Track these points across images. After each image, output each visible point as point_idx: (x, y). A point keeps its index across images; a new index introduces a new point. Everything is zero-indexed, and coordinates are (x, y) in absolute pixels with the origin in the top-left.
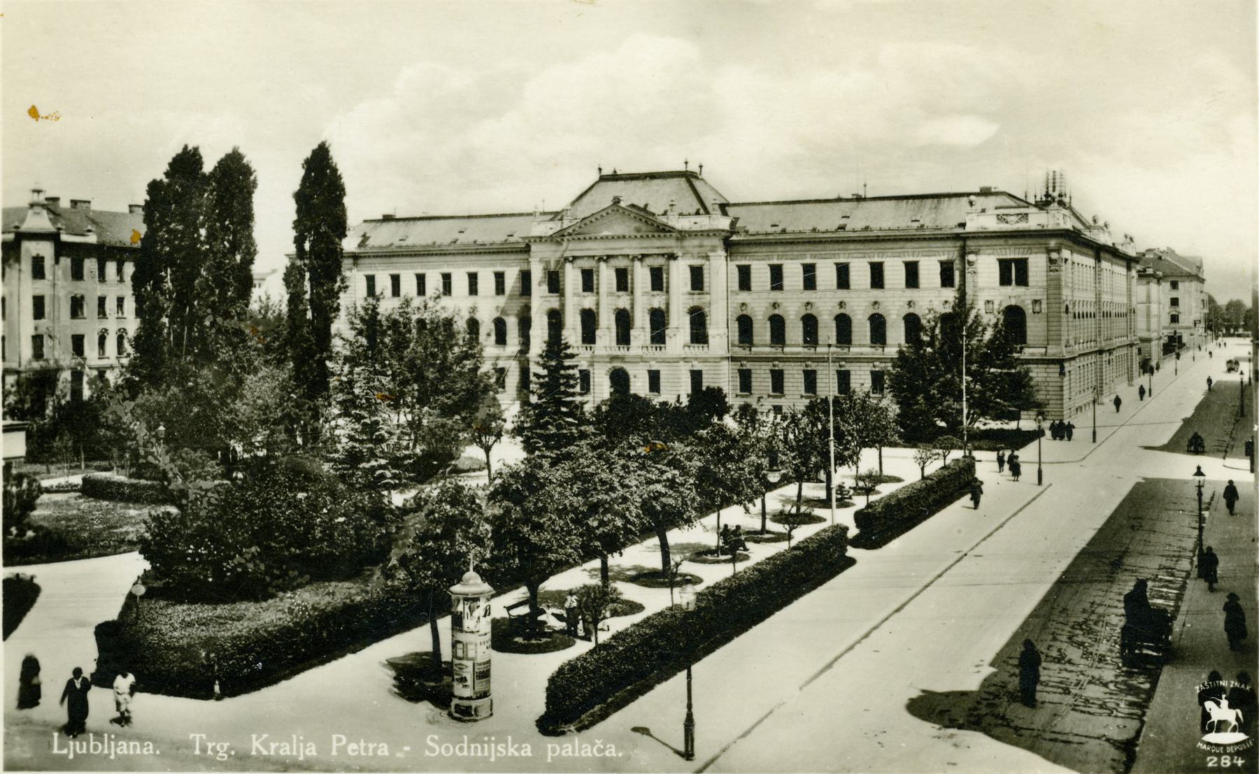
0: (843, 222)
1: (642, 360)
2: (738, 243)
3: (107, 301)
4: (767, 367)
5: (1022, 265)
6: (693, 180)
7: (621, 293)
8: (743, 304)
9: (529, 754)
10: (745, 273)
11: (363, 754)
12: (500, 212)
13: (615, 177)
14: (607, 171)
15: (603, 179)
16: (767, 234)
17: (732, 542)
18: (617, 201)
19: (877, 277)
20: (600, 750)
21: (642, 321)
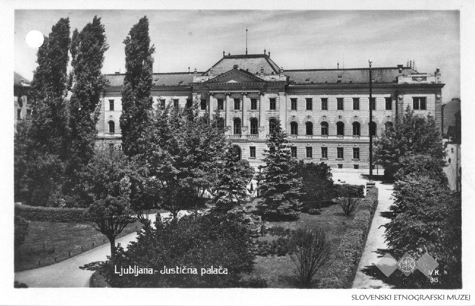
1: (247, 141)
2: (291, 88)
4: (304, 146)
5: (424, 100)
7: (236, 110)
8: (294, 116)
9: (196, 273)
10: (294, 101)
11: (177, 273)
12: (299, 69)
13: (230, 57)
14: (226, 54)
15: (225, 57)
16: (304, 84)
18: (236, 67)
20: (185, 271)
21: (247, 123)
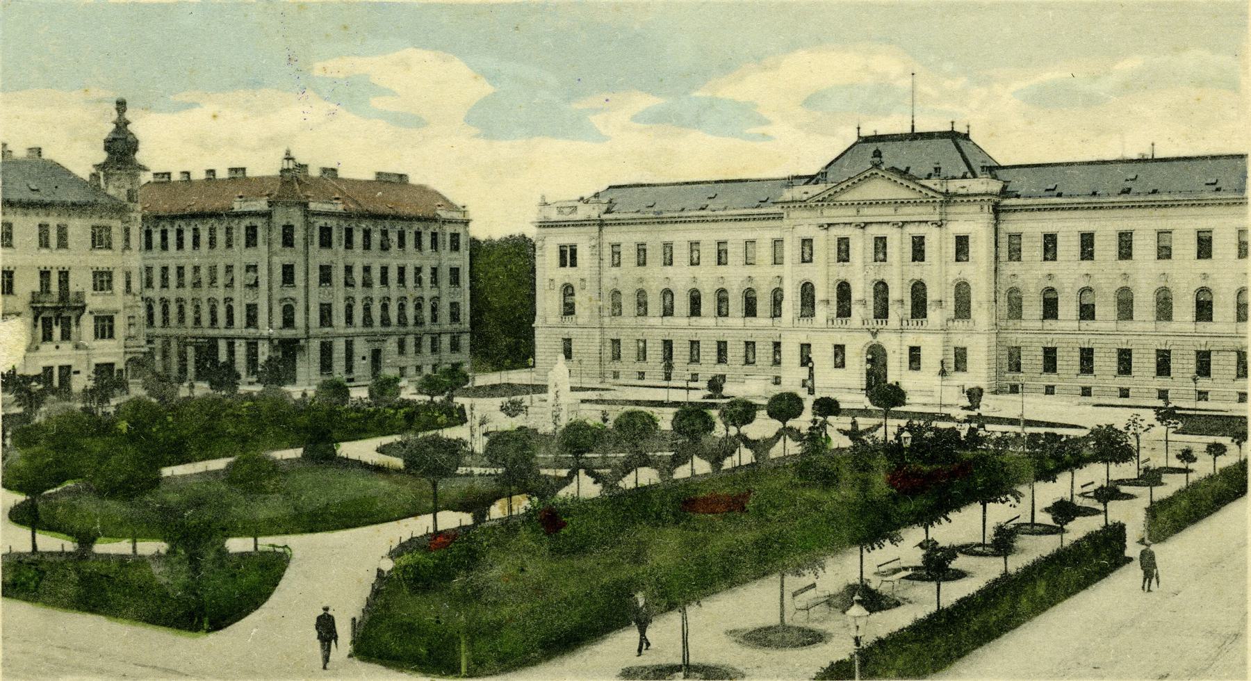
0: (1128, 185)
3: (390, 270)
6: (962, 143)
17: (937, 565)
19: (1125, 247)
